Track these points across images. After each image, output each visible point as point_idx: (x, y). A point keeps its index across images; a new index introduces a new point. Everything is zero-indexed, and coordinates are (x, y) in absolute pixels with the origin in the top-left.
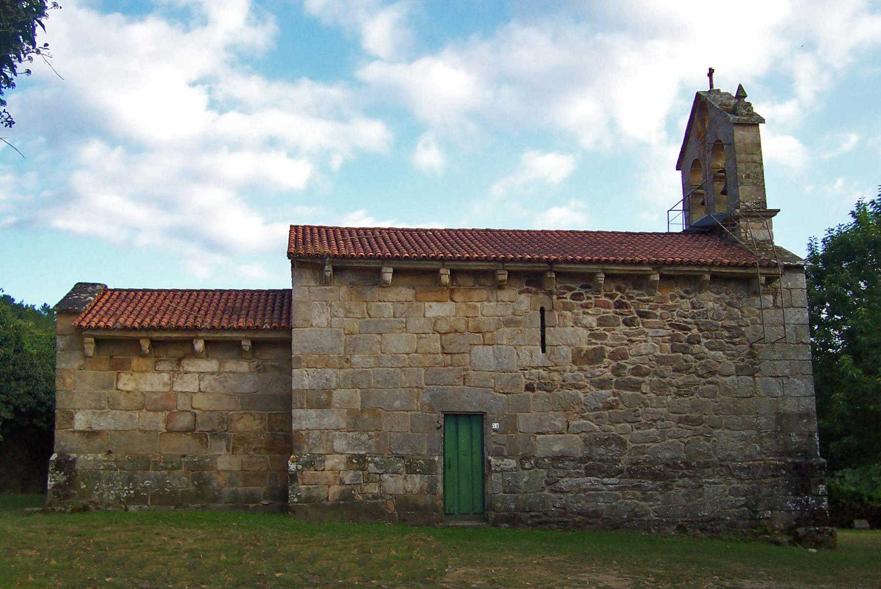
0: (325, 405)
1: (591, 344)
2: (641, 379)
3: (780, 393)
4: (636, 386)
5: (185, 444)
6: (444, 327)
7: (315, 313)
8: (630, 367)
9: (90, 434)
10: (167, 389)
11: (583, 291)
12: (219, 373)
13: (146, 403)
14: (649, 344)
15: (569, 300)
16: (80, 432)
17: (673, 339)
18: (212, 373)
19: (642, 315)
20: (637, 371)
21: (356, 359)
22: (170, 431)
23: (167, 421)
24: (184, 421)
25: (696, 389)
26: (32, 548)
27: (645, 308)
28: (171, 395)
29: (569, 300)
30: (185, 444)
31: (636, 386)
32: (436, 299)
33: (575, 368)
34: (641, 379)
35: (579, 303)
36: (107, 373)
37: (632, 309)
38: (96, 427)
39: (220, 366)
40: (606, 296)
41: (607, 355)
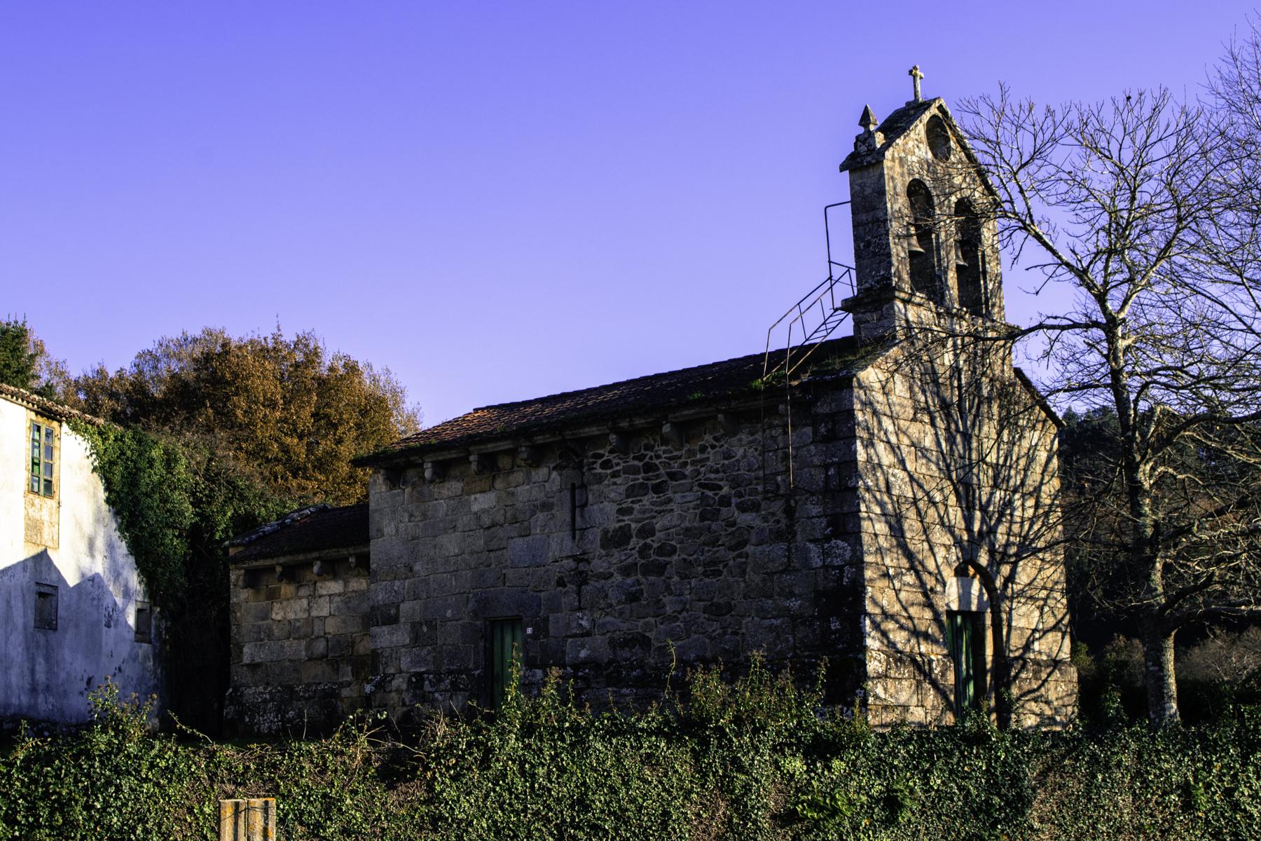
0: (392, 620)
1: (619, 521)
2: (667, 559)
3: (820, 564)
4: (660, 569)
5: (316, 671)
6: (486, 521)
7: (386, 522)
8: (655, 545)
9: (254, 666)
10: (306, 616)
11: (611, 457)
12: (344, 593)
13: (293, 630)
14: (677, 512)
15: (599, 471)
16: (247, 665)
17: (703, 497)
18: (339, 595)
19: (673, 476)
20: (661, 551)
21: (417, 567)
22: (310, 659)
23: (308, 648)
24: (320, 647)
25: (725, 566)
26: (792, 594)
27: (675, 466)
28: (310, 621)
29: (599, 471)
30: (316, 671)
31: (660, 569)
32: (478, 489)
33: (603, 552)
34: (667, 559)
35: (609, 471)
36: (264, 603)
37: (662, 471)
38: (257, 660)
39: (346, 585)
40: (634, 458)
41: (634, 533)
